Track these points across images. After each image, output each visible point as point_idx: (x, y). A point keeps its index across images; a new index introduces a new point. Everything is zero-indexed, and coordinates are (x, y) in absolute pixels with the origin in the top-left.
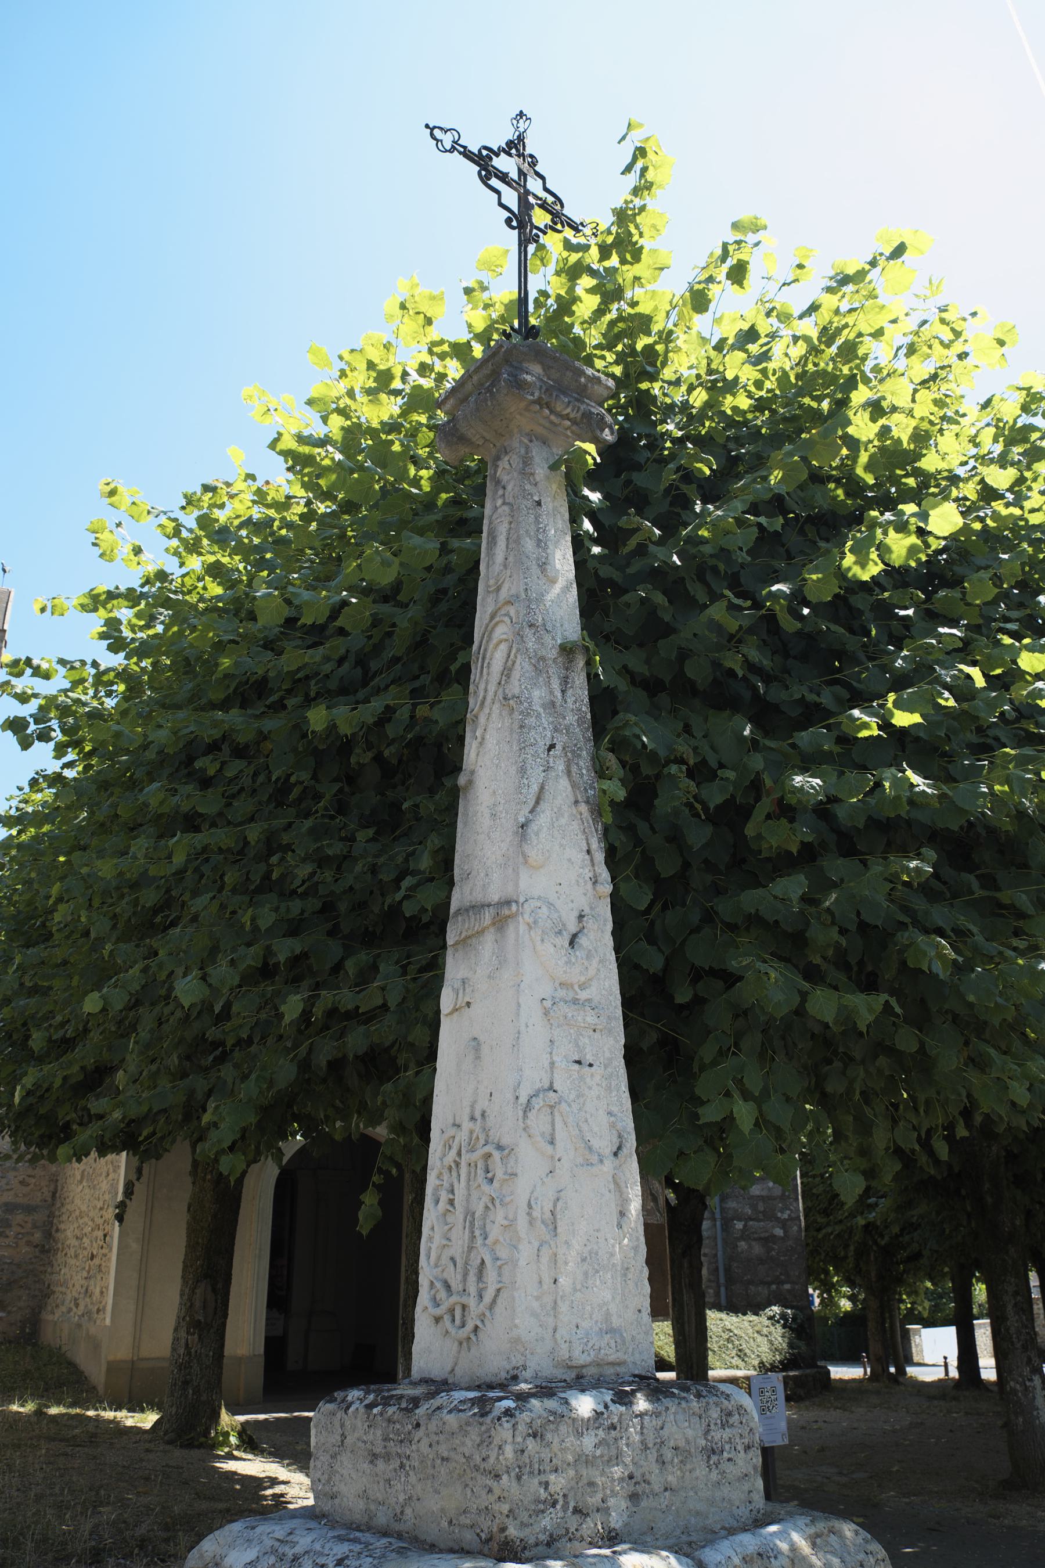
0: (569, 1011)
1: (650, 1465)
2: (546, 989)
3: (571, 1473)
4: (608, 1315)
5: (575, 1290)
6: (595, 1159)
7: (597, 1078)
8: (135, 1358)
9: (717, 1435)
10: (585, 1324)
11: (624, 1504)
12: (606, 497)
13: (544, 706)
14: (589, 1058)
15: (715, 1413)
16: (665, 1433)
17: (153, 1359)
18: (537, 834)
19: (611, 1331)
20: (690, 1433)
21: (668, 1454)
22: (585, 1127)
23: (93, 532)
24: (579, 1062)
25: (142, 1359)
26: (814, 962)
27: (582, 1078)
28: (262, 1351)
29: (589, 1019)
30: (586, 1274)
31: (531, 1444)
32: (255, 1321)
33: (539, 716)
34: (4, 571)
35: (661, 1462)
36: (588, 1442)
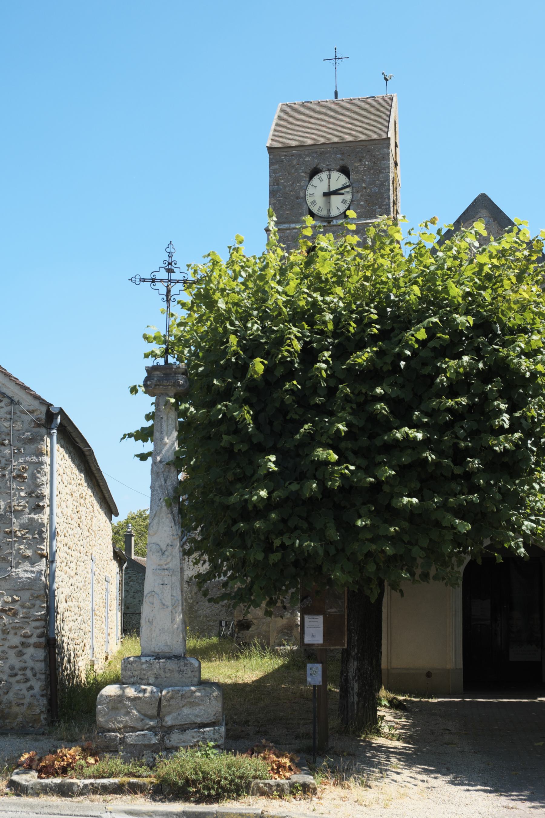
0: (160, 572)
1: (161, 672)
2: (154, 567)
3: (139, 672)
4: (166, 642)
5: (157, 636)
6: (165, 607)
7: (168, 588)
8: (389, 668)
9: (182, 668)
10: (160, 644)
11: (153, 679)
12: (222, 365)
13: (159, 487)
14: (166, 583)
15: (182, 664)
16: (166, 666)
17: (399, 669)
18: (152, 526)
19: (167, 646)
20: (174, 667)
21: (167, 671)
22: (163, 600)
23: (62, 480)
24: (163, 584)
25: (393, 669)
26: (505, 461)
27: (163, 588)
28: (461, 666)
29: (166, 573)
30: (160, 633)
31: (129, 666)
32: (456, 650)
33: (157, 490)
34: (386, 80)
35: (165, 672)
36: (144, 666)
